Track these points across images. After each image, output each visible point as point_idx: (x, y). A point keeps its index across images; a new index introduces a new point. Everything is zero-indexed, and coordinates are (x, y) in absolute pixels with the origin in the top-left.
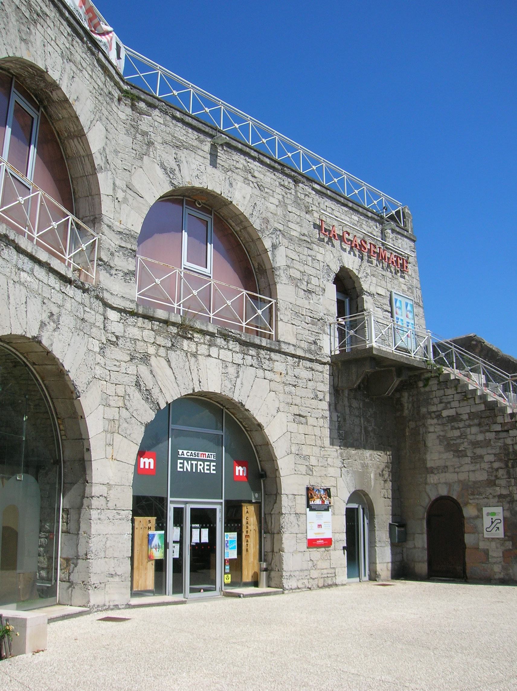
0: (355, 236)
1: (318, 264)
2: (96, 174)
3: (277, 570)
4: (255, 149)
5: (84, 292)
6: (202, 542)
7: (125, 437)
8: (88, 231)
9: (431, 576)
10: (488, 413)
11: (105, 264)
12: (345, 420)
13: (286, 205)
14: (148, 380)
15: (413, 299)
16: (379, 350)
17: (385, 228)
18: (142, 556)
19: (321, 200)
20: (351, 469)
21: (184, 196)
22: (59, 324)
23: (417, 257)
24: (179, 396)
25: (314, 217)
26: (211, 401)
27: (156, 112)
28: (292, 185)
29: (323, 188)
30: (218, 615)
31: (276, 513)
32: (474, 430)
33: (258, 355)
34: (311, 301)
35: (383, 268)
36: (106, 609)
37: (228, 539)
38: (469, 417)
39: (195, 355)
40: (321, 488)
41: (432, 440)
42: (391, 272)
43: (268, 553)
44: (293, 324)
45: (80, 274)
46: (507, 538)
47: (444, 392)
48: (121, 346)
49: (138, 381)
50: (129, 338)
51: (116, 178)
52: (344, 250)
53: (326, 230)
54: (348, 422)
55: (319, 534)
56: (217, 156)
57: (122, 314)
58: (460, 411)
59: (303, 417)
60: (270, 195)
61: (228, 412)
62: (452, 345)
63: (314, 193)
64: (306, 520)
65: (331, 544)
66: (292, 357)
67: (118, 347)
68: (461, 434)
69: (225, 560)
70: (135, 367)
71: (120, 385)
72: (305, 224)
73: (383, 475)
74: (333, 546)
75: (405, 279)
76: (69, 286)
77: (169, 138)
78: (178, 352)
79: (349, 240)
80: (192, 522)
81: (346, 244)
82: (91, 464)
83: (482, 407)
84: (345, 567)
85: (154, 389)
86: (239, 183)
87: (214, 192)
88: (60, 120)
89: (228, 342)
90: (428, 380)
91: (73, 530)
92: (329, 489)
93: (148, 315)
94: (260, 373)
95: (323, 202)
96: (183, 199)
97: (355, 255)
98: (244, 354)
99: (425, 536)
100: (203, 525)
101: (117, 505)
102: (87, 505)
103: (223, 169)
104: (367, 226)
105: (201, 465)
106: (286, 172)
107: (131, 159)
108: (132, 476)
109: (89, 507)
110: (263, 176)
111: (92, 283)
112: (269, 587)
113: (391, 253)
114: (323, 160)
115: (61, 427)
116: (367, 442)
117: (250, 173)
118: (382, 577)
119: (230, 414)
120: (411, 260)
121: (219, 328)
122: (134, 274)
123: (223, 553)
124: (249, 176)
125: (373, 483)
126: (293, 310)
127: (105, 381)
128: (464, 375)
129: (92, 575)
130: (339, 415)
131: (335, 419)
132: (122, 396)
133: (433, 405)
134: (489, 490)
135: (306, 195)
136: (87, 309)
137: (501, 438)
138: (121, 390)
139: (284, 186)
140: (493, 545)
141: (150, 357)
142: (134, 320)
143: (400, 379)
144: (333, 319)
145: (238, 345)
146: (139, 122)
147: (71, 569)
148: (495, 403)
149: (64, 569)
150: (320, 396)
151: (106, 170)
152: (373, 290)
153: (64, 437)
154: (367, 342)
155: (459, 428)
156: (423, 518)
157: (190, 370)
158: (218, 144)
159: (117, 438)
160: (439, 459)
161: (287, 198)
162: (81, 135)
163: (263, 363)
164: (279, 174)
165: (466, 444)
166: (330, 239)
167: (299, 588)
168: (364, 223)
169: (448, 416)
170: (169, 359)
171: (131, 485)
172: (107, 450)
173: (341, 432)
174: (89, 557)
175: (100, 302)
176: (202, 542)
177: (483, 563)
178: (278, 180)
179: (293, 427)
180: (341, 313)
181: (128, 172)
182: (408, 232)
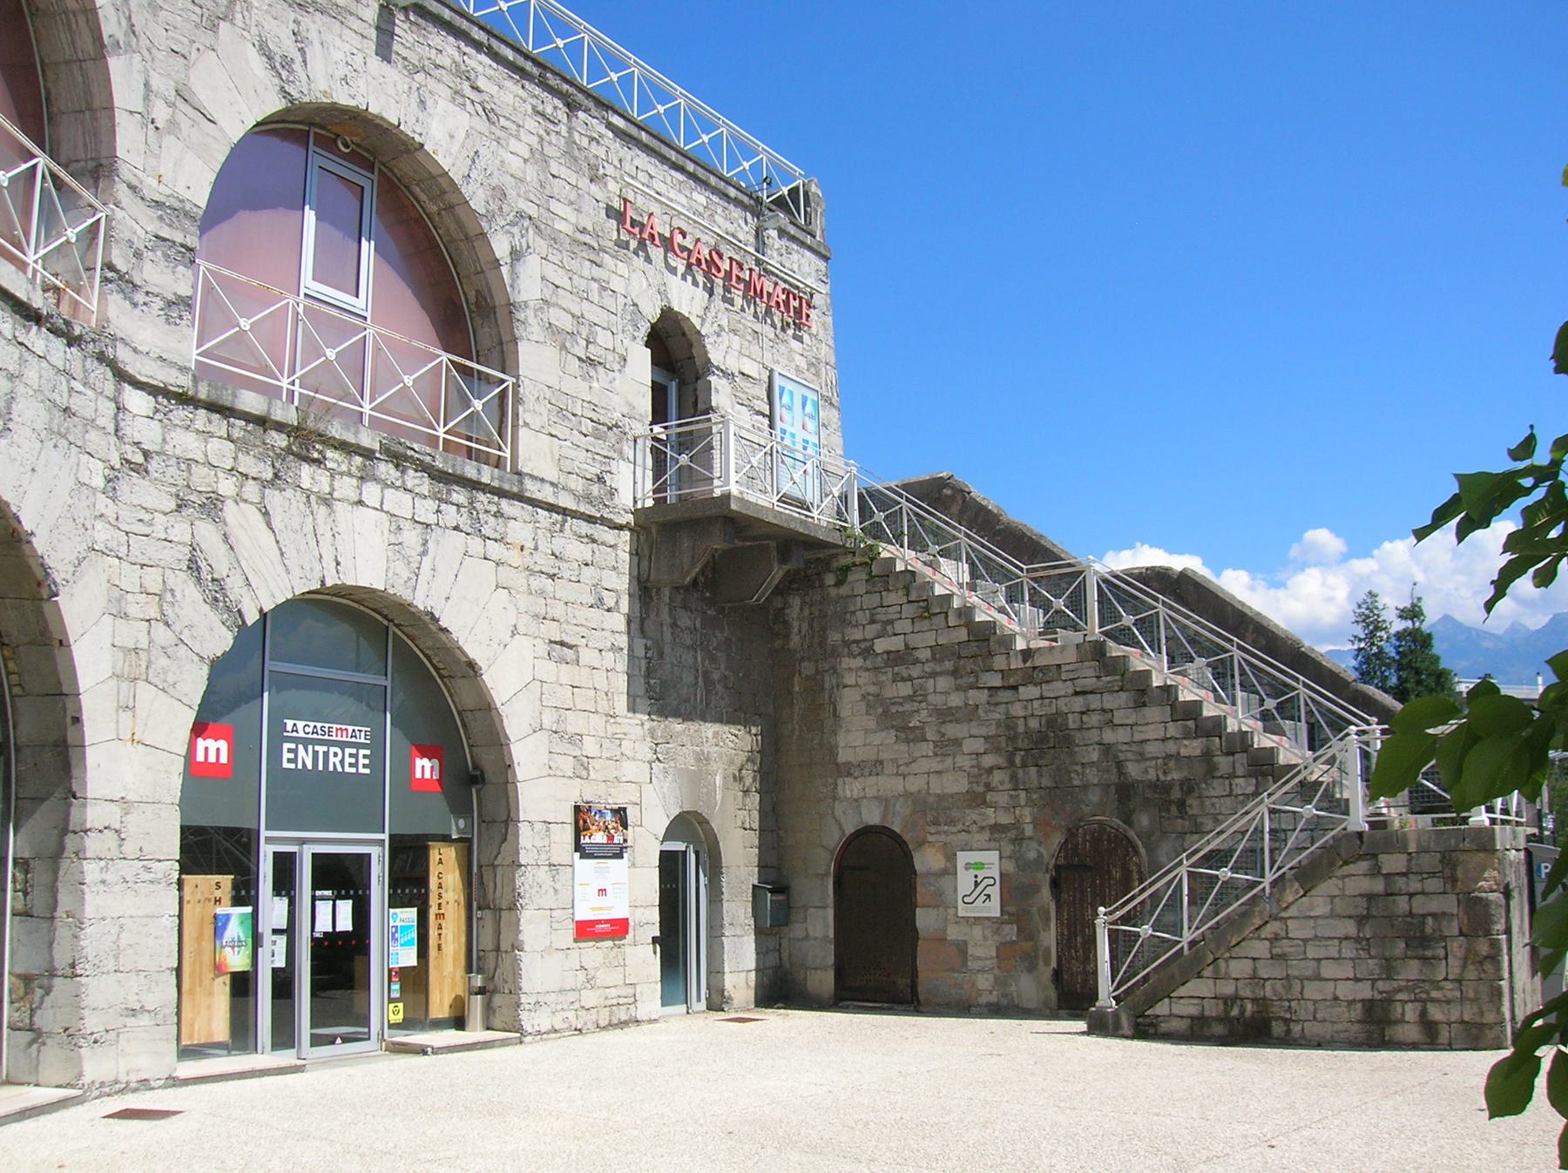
0: (698, 240)
1: (613, 299)
2: (105, 57)
3: (506, 991)
4: (482, 23)
5: (69, 345)
6: (338, 930)
7: (163, 690)
8: (81, 197)
9: (842, 1000)
10: (974, 648)
11: (121, 278)
12: (661, 656)
13: (547, 159)
14: (217, 558)
15: (818, 389)
16: (741, 500)
17: (766, 225)
18: (201, 967)
19: (625, 152)
20: (673, 765)
21: (311, 124)
22: (10, 419)
23: (831, 295)
24: (290, 596)
25: (609, 191)
26: (362, 608)
28: (561, 115)
29: (800, 231)
30: (383, 1097)
31: (506, 863)
32: (943, 683)
33: (471, 503)
34: (595, 384)
35: (755, 315)
36: (121, 1091)
37: (398, 923)
38: (933, 655)
40: (605, 808)
41: (850, 703)
42: (773, 325)
43: (487, 954)
44: (552, 435)
45: (58, 300)
46: (1006, 917)
47: (881, 599)
48: (156, 475)
49: (193, 558)
50: (174, 456)
51: (152, 72)
52: (673, 271)
53: (634, 223)
54: (667, 659)
55: (601, 909)
56: (393, 34)
57: (160, 399)
58: (914, 641)
59: (570, 647)
60: (511, 134)
61: (399, 633)
62: (901, 496)
63: (610, 135)
64: (573, 879)
65: (627, 933)
66: (547, 510)
67: (147, 478)
68: (915, 693)
69: (390, 971)
70: (187, 526)
71: (151, 566)
72: (588, 205)
73: (741, 779)
74: (630, 937)
75: (802, 343)
76: (35, 328)
78: (289, 493)
79: (683, 248)
80: (315, 887)
81: (677, 256)
82: (84, 753)
83: (963, 635)
84: (656, 982)
85: (232, 578)
86: (440, 101)
87: (382, 118)
89: (403, 472)
90: (845, 570)
91: (39, 907)
92: (624, 809)
93: (221, 402)
94: (476, 544)
95: (629, 158)
96: (309, 131)
97: (695, 283)
98: (440, 500)
99: (831, 912)
100: (339, 892)
101: (144, 849)
102: (74, 850)
103: (405, 67)
104: (726, 219)
105: (336, 755)
106: (550, 82)
107: (188, 26)
108: (178, 782)
109: (79, 854)
110: (497, 88)
111: (89, 322)
112: (488, 1029)
113: (776, 284)
114: (635, 61)
115: (11, 665)
116: (707, 705)
117: (468, 79)
118: (736, 1002)
119: (405, 638)
120: (817, 300)
121: (384, 438)
122: (189, 305)
123: (385, 954)
124: (464, 88)
125: (719, 797)
126: (553, 402)
127: (117, 557)
128: (925, 563)
129: (86, 1013)
130: (649, 643)
131: (640, 652)
132: (155, 594)
133: (857, 626)
134: (972, 815)
135: (592, 139)
136: (77, 386)
137: (1001, 703)
138: (153, 580)
139: (542, 115)
140: (977, 932)
141: (223, 502)
142: (186, 413)
143: (786, 567)
144: (641, 424)
145: (427, 480)
147: (37, 998)
148: (991, 626)
149: (18, 1001)
150: (610, 600)
151: (130, 49)
152: (732, 364)
153: (16, 690)
154: (716, 483)
155: (910, 679)
156: (826, 874)
157: (316, 535)
158: (395, 5)
159: (145, 692)
160: (865, 745)
161: (550, 143)
163: (482, 522)
164: (533, 86)
165: (924, 713)
166: (642, 243)
167: (556, 1031)
169: (888, 653)
170: (268, 508)
171: (177, 801)
172: (121, 720)
173: (652, 682)
174: (79, 972)
175: (108, 368)
176: (338, 930)
177: (953, 970)
178: (531, 100)
179: (548, 670)
180: (659, 414)
181: (182, 60)
182: (814, 237)
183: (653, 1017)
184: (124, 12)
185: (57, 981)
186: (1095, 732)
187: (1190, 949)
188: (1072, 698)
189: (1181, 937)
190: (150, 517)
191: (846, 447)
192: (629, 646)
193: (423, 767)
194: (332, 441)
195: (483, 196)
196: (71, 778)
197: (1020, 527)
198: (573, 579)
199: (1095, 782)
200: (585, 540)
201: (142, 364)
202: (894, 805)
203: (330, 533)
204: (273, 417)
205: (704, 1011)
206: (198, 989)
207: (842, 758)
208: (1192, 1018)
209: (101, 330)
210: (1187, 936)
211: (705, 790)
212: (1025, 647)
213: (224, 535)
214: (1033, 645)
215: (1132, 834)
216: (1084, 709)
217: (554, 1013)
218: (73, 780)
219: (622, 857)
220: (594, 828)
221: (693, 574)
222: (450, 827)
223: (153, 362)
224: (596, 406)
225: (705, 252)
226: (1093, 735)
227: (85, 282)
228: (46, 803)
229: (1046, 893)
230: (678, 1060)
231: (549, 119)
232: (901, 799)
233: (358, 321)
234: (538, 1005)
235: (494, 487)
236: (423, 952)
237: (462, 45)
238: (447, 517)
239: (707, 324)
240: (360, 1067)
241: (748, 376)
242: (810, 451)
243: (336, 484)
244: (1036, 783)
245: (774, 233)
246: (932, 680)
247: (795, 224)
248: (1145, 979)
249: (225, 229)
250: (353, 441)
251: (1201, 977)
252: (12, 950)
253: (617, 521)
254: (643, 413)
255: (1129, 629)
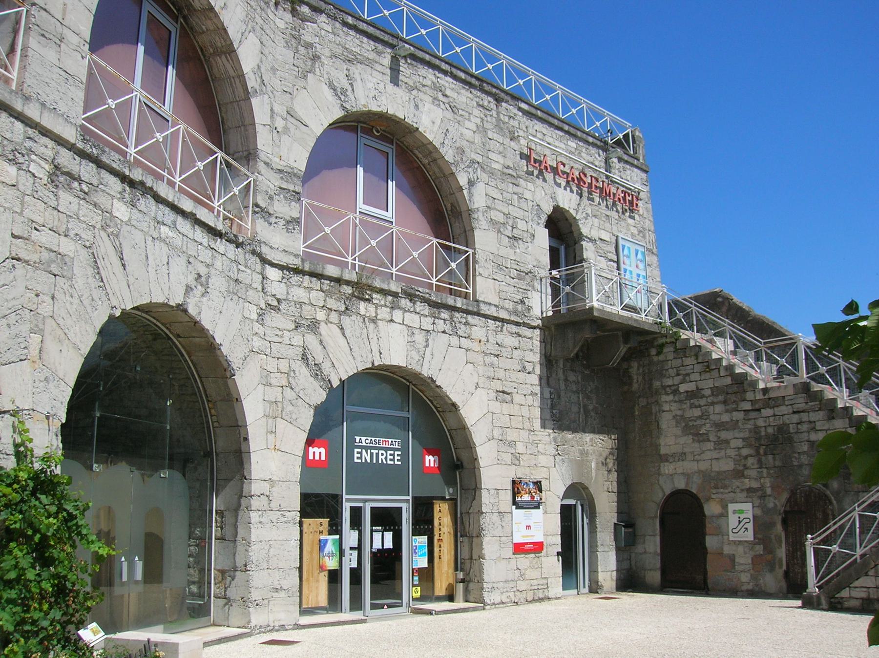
0: (572, 167)
1: (526, 203)
2: (249, 98)
3: (476, 581)
4: (447, 60)
5: (237, 247)
6: (385, 548)
7: (290, 422)
8: (241, 171)
10: (735, 388)
11: (263, 210)
12: (559, 397)
15: (644, 245)
19: (529, 123)
20: (567, 457)
21: (359, 122)
22: (208, 287)
23: (650, 192)
25: (521, 145)
26: (395, 376)
27: (323, 18)
28: (493, 105)
30: (405, 636)
31: (475, 511)
32: (719, 408)
33: (451, 318)
35: (607, 206)
36: (270, 631)
37: (417, 544)
38: (712, 393)
39: (374, 321)
40: (529, 481)
41: (666, 421)
42: (617, 211)
44: (495, 279)
45: (232, 224)
50: (293, 301)
51: (274, 103)
52: (559, 185)
53: (535, 161)
54: (563, 399)
55: (527, 536)
56: (399, 71)
57: (285, 271)
58: (702, 385)
59: (508, 394)
61: (416, 389)
63: (520, 114)
64: (512, 520)
65: (542, 549)
66: (493, 320)
69: (413, 569)
70: (301, 337)
72: (510, 153)
73: (606, 464)
75: (634, 220)
76: (219, 240)
77: (339, 50)
78: (354, 317)
79: (564, 173)
83: (728, 381)
84: (559, 577)
86: (426, 104)
87: (396, 116)
88: (204, 32)
89: (414, 303)
91: (229, 535)
92: (540, 482)
93: (316, 272)
94: (454, 340)
95: (531, 125)
96: (357, 127)
97: (572, 191)
98: (435, 317)
99: (658, 538)
100: (385, 528)
102: (245, 506)
103: (406, 88)
104: (587, 154)
105: (382, 454)
107: (292, 78)
109: (248, 508)
110: (456, 94)
111: (247, 234)
112: (466, 601)
113: (618, 188)
115: (213, 411)
116: (586, 423)
117: (441, 91)
118: (605, 588)
120: (642, 195)
121: (403, 286)
122: (298, 222)
123: (410, 561)
125: (594, 475)
127: (265, 354)
128: (707, 341)
129: (252, 590)
131: (547, 395)
133: (669, 377)
134: (736, 483)
136: (242, 268)
138: (284, 365)
139: (482, 106)
140: (741, 549)
141: (319, 323)
143: (629, 346)
145: (427, 307)
146: (302, 31)
147: (228, 583)
148: (745, 375)
150: (529, 367)
151: (263, 93)
152: (594, 234)
153: (216, 424)
154: (587, 301)
155: (700, 406)
156: (656, 517)
157: (368, 339)
158: (400, 56)
159: (281, 424)
160: (675, 444)
161: (487, 121)
162: (230, 51)
163: (458, 328)
165: (708, 425)
166: (541, 172)
167: (503, 603)
168: (584, 150)
169: (687, 392)
171: (298, 480)
173: (554, 411)
174: (248, 569)
176: (385, 548)
177: (727, 571)
179: (496, 406)
180: (555, 263)
181: (289, 95)
182: (638, 160)
183: (558, 596)
184: (258, 75)
185: (238, 573)
186: (806, 434)
187: (861, 559)
188: (792, 415)
189: (855, 552)
190: (282, 333)
191: (662, 277)
192: (541, 392)
193: (430, 460)
194: (375, 289)
195: (452, 153)
196: (244, 469)
197: (762, 318)
198: (509, 357)
199: (806, 463)
200: (515, 335)
201: (274, 254)
202: (693, 478)
203: (376, 338)
204: (344, 278)
205: (587, 593)
206: (311, 578)
207: (663, 451)
208: (862, 599)
209: (253, 239)
210: (859, 551)
211: (586, 471)
212: (764, 387)
213: (320, 341)
214: (769, 385)
215: (828, 492)
216: (799, 421)
217: (502, 593)
218: (245, 470)
219: (539, 508)
220: (523, 492)
221: (575, 352)
222: (445, 493)
223: (280, 253)
224: (518, 262)
225: (577, 173)
226: (805, 436)
227: (244, 214)
228: (232, 481)
229: (779, 527)
230: (567, 619)
231: (486, 109)
232: (697, 474)
233: (387, 225)
234: (493, 589)
235: (464, 309)
236: (431, 560)
237: (437, 73)
238: (439, 326)
239: (579, 213)
240: (395, 621)
241: (604, 240)
242: (641, 281)
243: (379, 312)
244: (772, 464)
245: (615, 160)
246: (712, 407)
247: (628, 155)
248: (838, 574)
249: (316, 181)
250: (387, 289)
251: (868, 576)
252: (215, 557)
253: (532, 324)
254: (545, 265)
255: (824, 375)
